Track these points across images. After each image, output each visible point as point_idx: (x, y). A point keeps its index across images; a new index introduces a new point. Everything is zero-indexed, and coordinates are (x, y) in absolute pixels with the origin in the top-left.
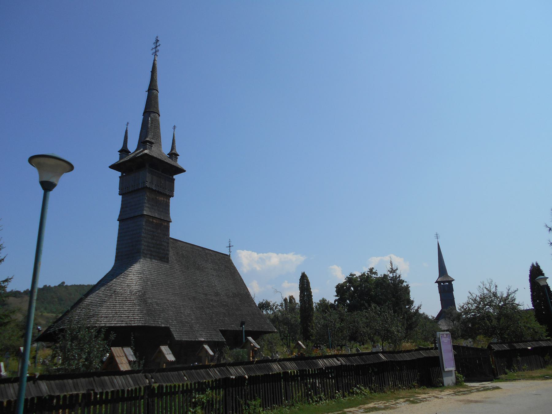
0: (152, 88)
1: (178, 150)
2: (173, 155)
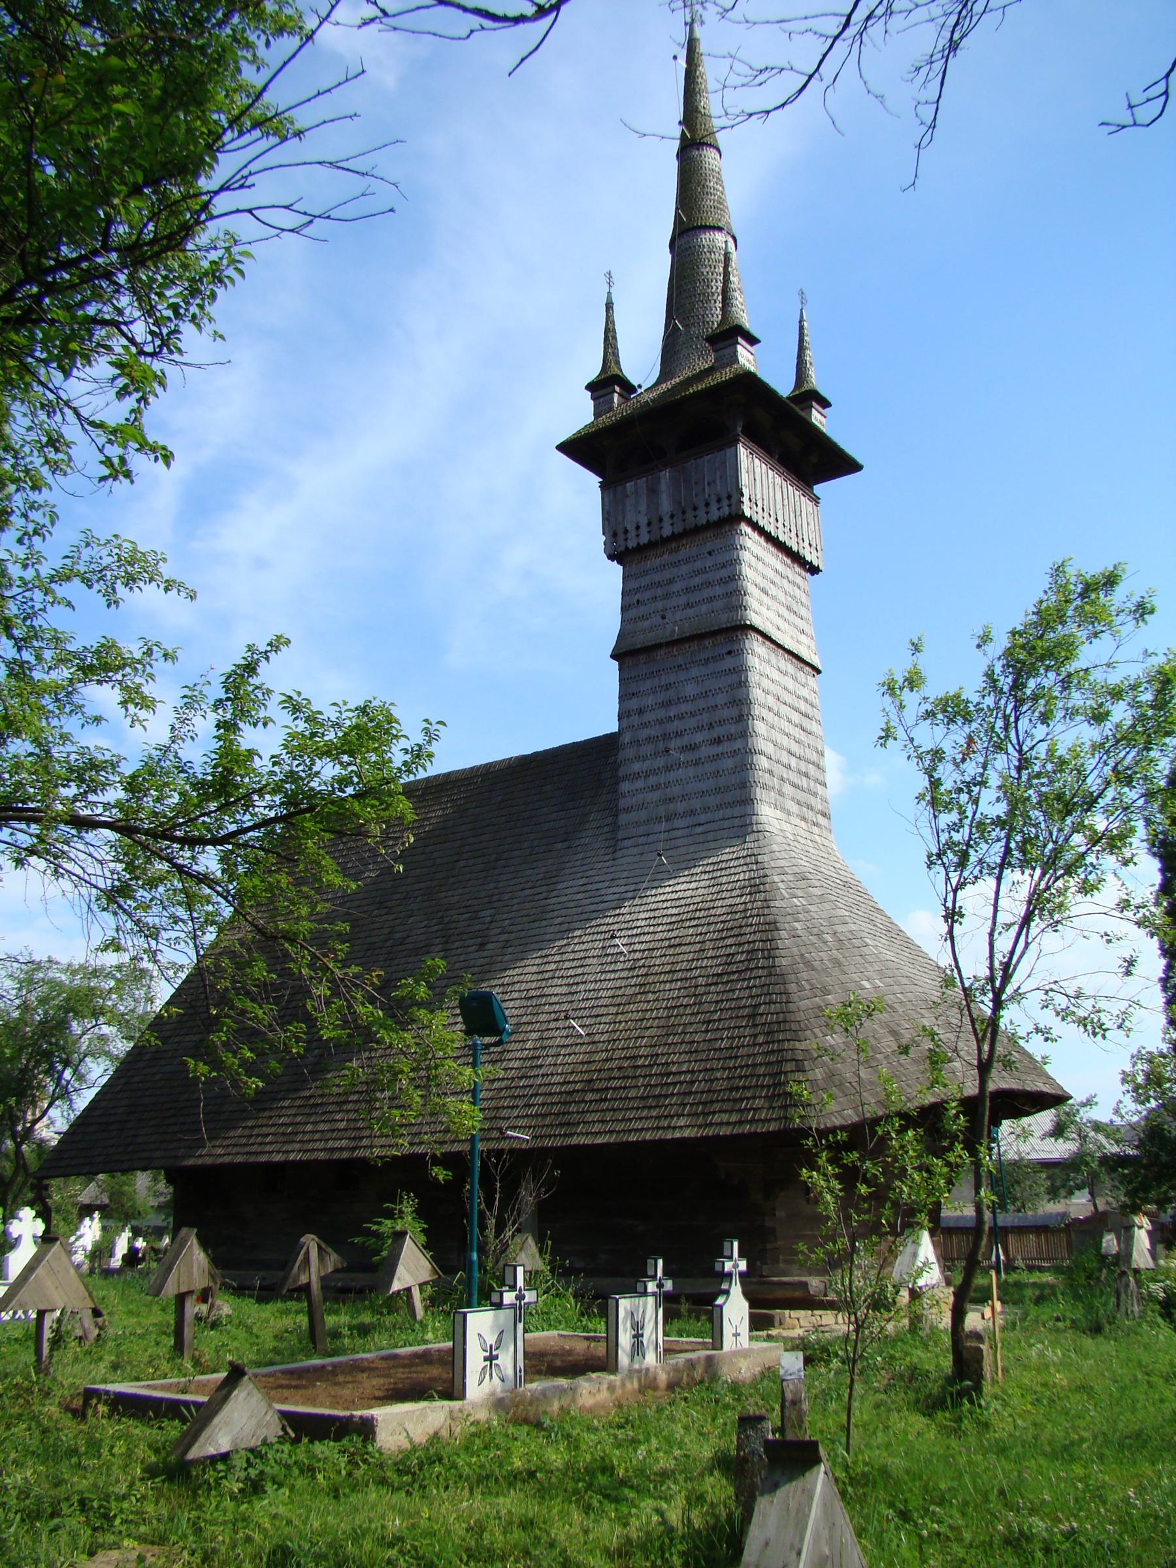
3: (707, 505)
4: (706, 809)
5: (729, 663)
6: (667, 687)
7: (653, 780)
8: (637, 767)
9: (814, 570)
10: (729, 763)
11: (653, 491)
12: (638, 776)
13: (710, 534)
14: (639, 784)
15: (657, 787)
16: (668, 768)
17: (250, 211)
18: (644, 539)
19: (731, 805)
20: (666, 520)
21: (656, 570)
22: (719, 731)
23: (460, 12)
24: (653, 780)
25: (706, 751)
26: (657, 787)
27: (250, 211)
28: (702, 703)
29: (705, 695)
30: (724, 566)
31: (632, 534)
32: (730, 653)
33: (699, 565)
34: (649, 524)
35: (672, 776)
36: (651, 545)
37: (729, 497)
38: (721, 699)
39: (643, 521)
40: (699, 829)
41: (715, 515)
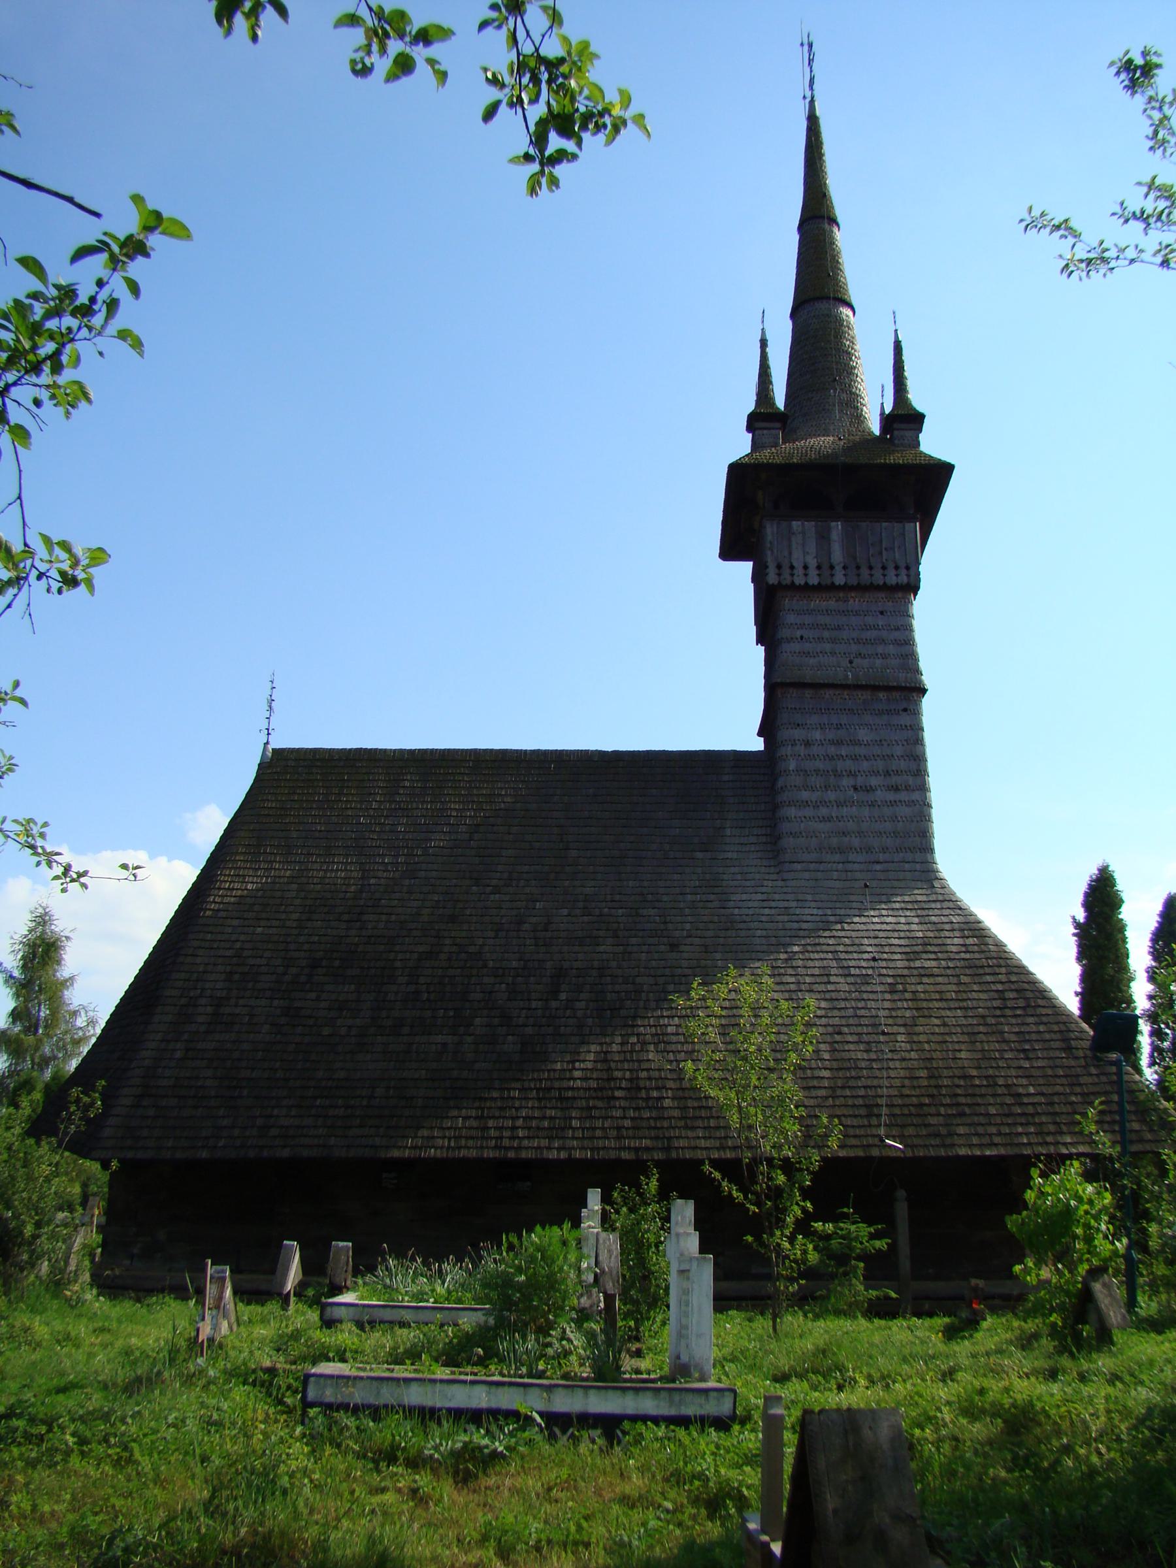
0: (817, 217)
1: (917, 399)
2: (905, 420)
3: (884, 568)
4: (884, 850)
5: (905, 719)
6: (839, 726)
7: (824, 811)
8: (805, 795)
9: (97, 215)
10: (904, 811)
11: (823, 537)
12: (806, 804)
13: (882, 595)
14: (808, 812)
15: (829, 819)
16: (839, 804)
17: (20, 497)
18: (814, 580)
19: (911, 850)
20: (838, 568)
21: (828, 612)
22: (894, 780)
23: (77, 200)
24: (824, 811)
25: (880, 795)
26: (829, 819)
27: (20, 497)
28: (877, 750)
29: (880, 743)
30: (897, 629)
31: (799, 571)
32: (905, 710)
33: (869, 620)
34: (819, 567)
35: (845, 811)
36: (819, 588)
37: (908, 568)
38: (898, 750)
39: (812, 563)
40: (878, 867)
41: (892, 579)
